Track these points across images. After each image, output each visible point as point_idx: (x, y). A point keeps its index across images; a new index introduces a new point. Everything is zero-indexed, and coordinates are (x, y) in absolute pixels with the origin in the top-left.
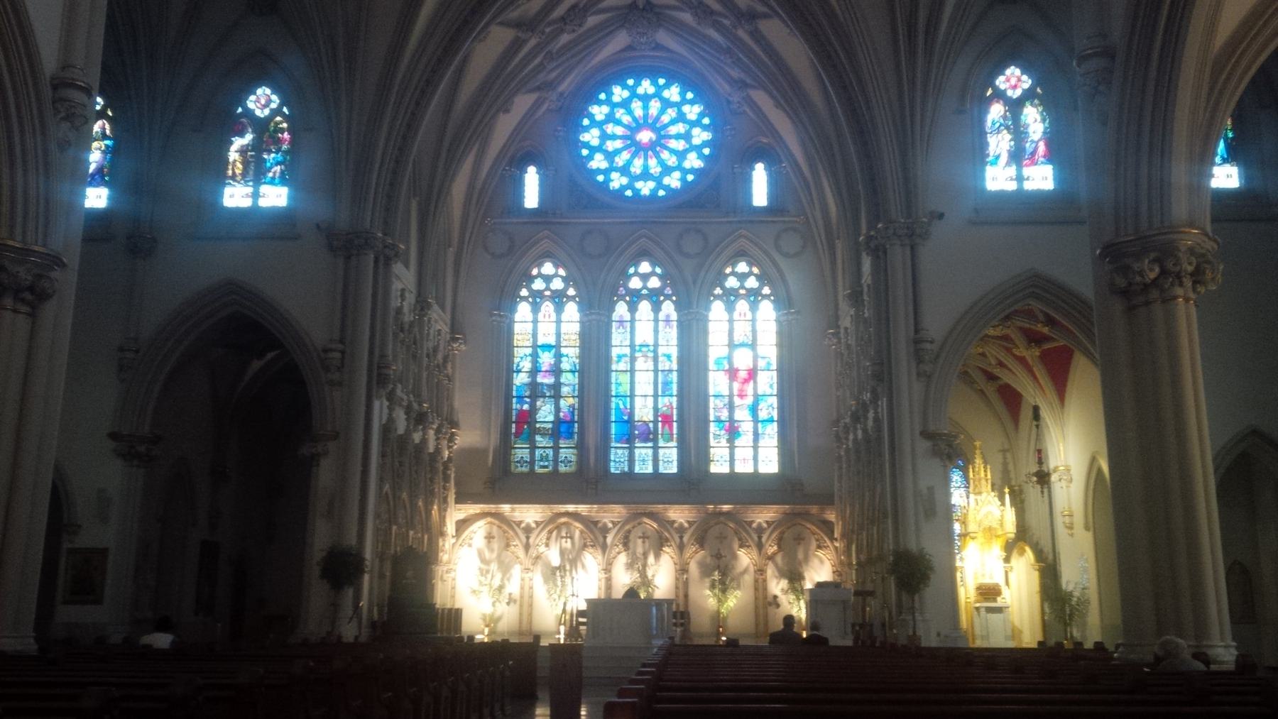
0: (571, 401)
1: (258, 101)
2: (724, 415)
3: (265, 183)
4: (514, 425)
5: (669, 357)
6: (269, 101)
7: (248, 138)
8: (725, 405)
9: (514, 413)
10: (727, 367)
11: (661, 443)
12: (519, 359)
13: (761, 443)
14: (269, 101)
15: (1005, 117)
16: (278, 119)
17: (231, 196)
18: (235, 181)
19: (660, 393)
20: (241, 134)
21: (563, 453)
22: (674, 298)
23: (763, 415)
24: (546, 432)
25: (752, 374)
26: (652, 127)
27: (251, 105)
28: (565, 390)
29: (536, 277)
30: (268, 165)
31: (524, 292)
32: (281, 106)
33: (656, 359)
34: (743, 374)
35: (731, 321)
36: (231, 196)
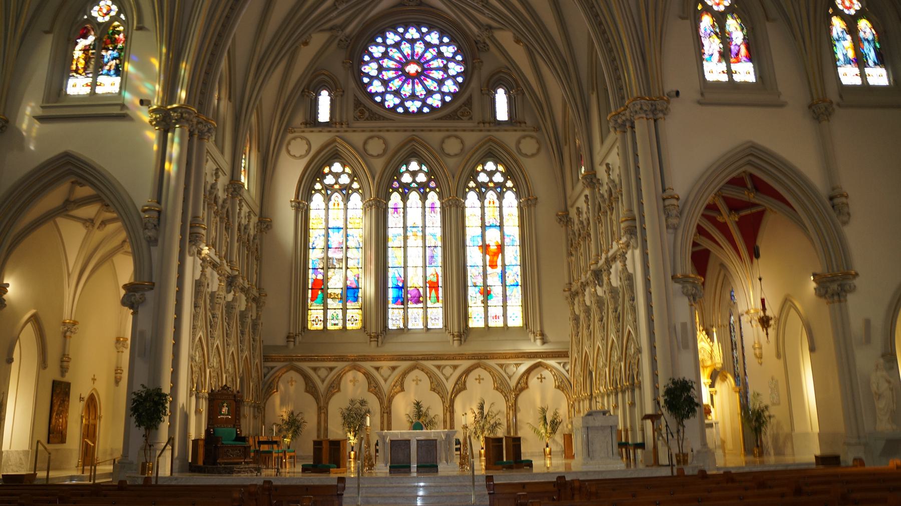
0: (356, 271)
1: (101, 10)
2: (480, 282)
3: (102, 74)
4: (310, 291)
5: (434, 235)
6: (109, 11)
7: (91, 39)
8: (479, 273)
9: (310, 282)
10: (480, 244)
11: (429, 304)
12: (314, 239)
13: (509, 303)
14: (109, 11)
15: (713, 26)
16: (116, 23)
17: (74, 86)
18: (77, 73)
19: (427, 265)
20: (85, 37)
21: (350, 313)
22: (437, 190)
23: (509, 281)
24: (336, 297)
25: (501, 248)
26: (418, 63)
27: (94, 13)
28: (351, 263)
29: (327, 174)
30: (106, 60)
31: (318, 186)
32: (118, 14)
33: (424, 237)
34: (493, 248)
35: (483, 207)
36: (74, 86)
